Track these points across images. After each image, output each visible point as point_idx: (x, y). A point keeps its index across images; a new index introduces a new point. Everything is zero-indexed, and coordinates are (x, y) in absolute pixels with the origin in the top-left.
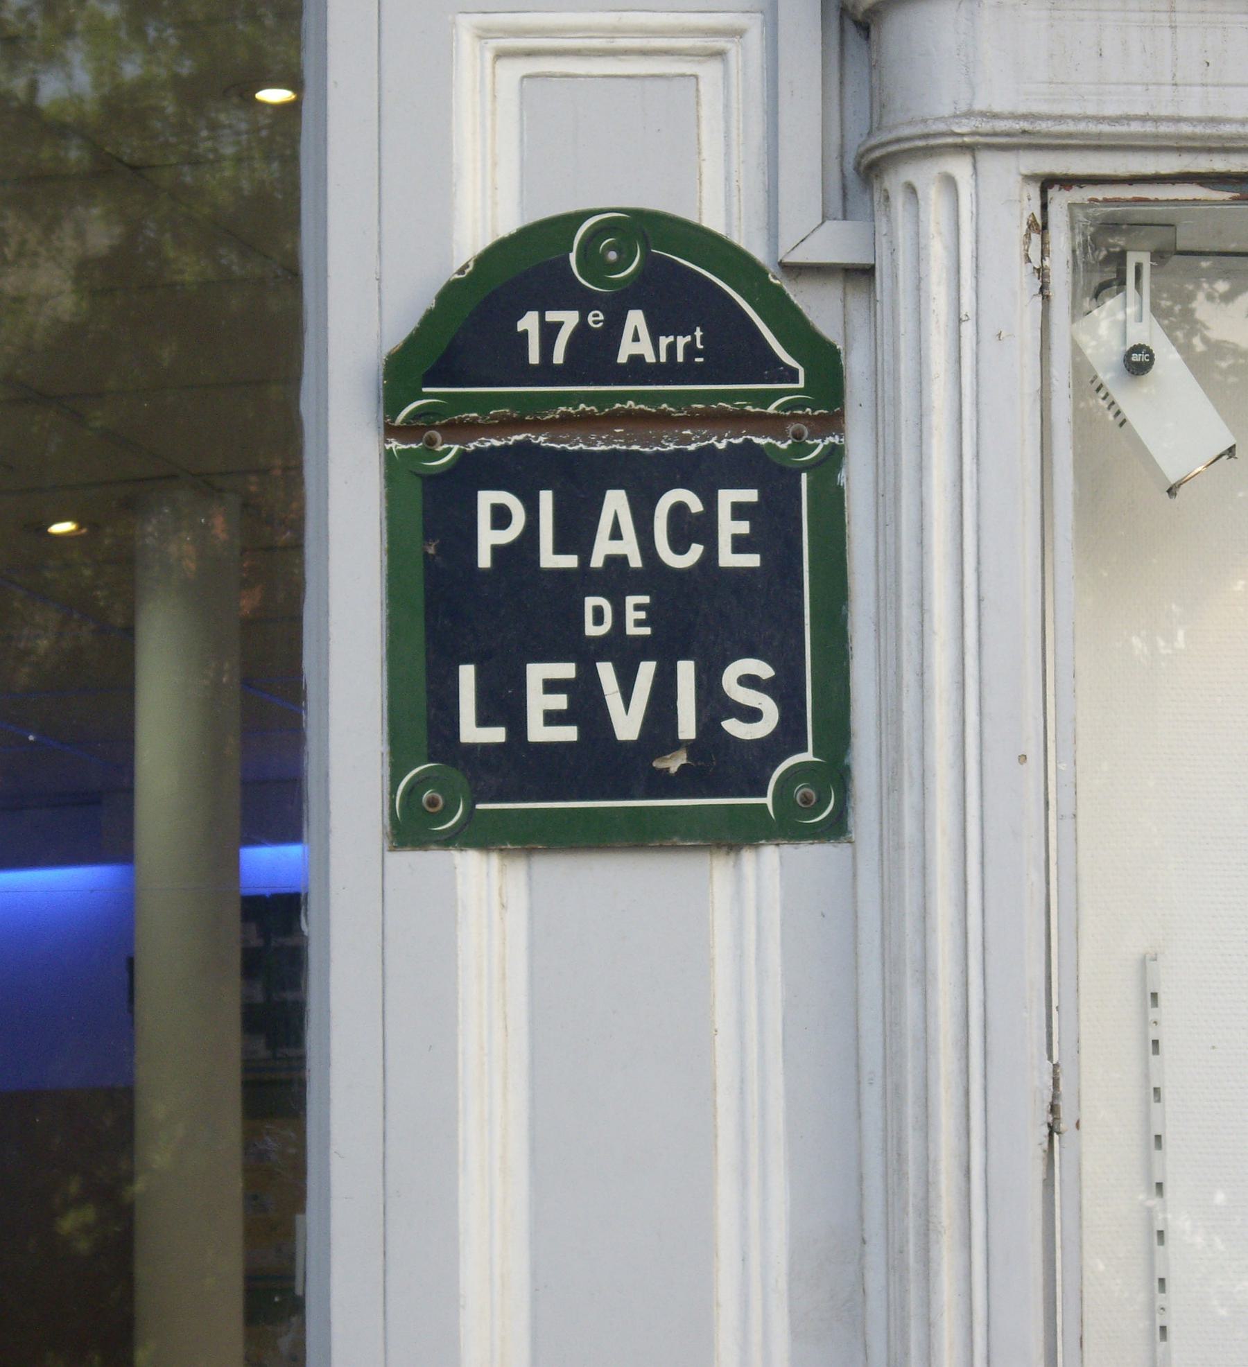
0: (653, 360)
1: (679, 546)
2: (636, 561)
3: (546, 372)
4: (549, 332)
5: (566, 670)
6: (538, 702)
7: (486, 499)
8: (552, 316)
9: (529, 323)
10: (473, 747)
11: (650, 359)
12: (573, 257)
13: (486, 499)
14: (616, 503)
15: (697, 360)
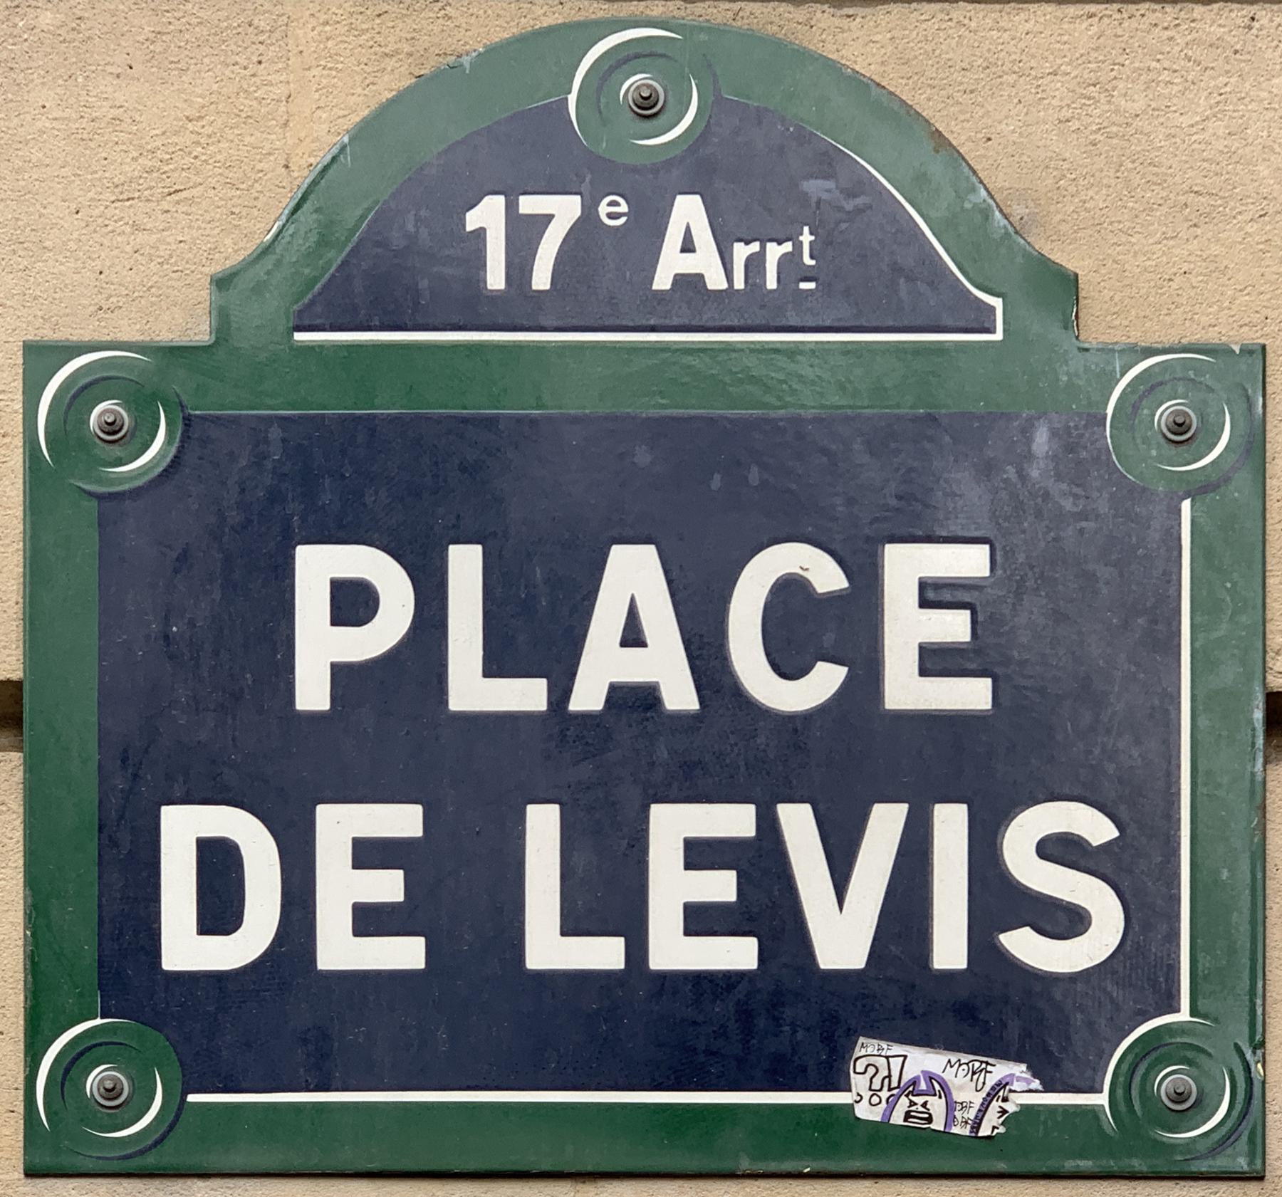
0: (724, 285)
1: (788, 665)
2: (680, 695)
3: (519, 307)
4: (524, 234)
5: (737, 821)
6: (672, 887)
7: (317, 567)
8: (530, 205)
9: (488, 215)
10: (544, 978)
11: (716, 281)
12: (572, 99)
13: (317, 567)
14: (633, 575)
15: (804, 286)
